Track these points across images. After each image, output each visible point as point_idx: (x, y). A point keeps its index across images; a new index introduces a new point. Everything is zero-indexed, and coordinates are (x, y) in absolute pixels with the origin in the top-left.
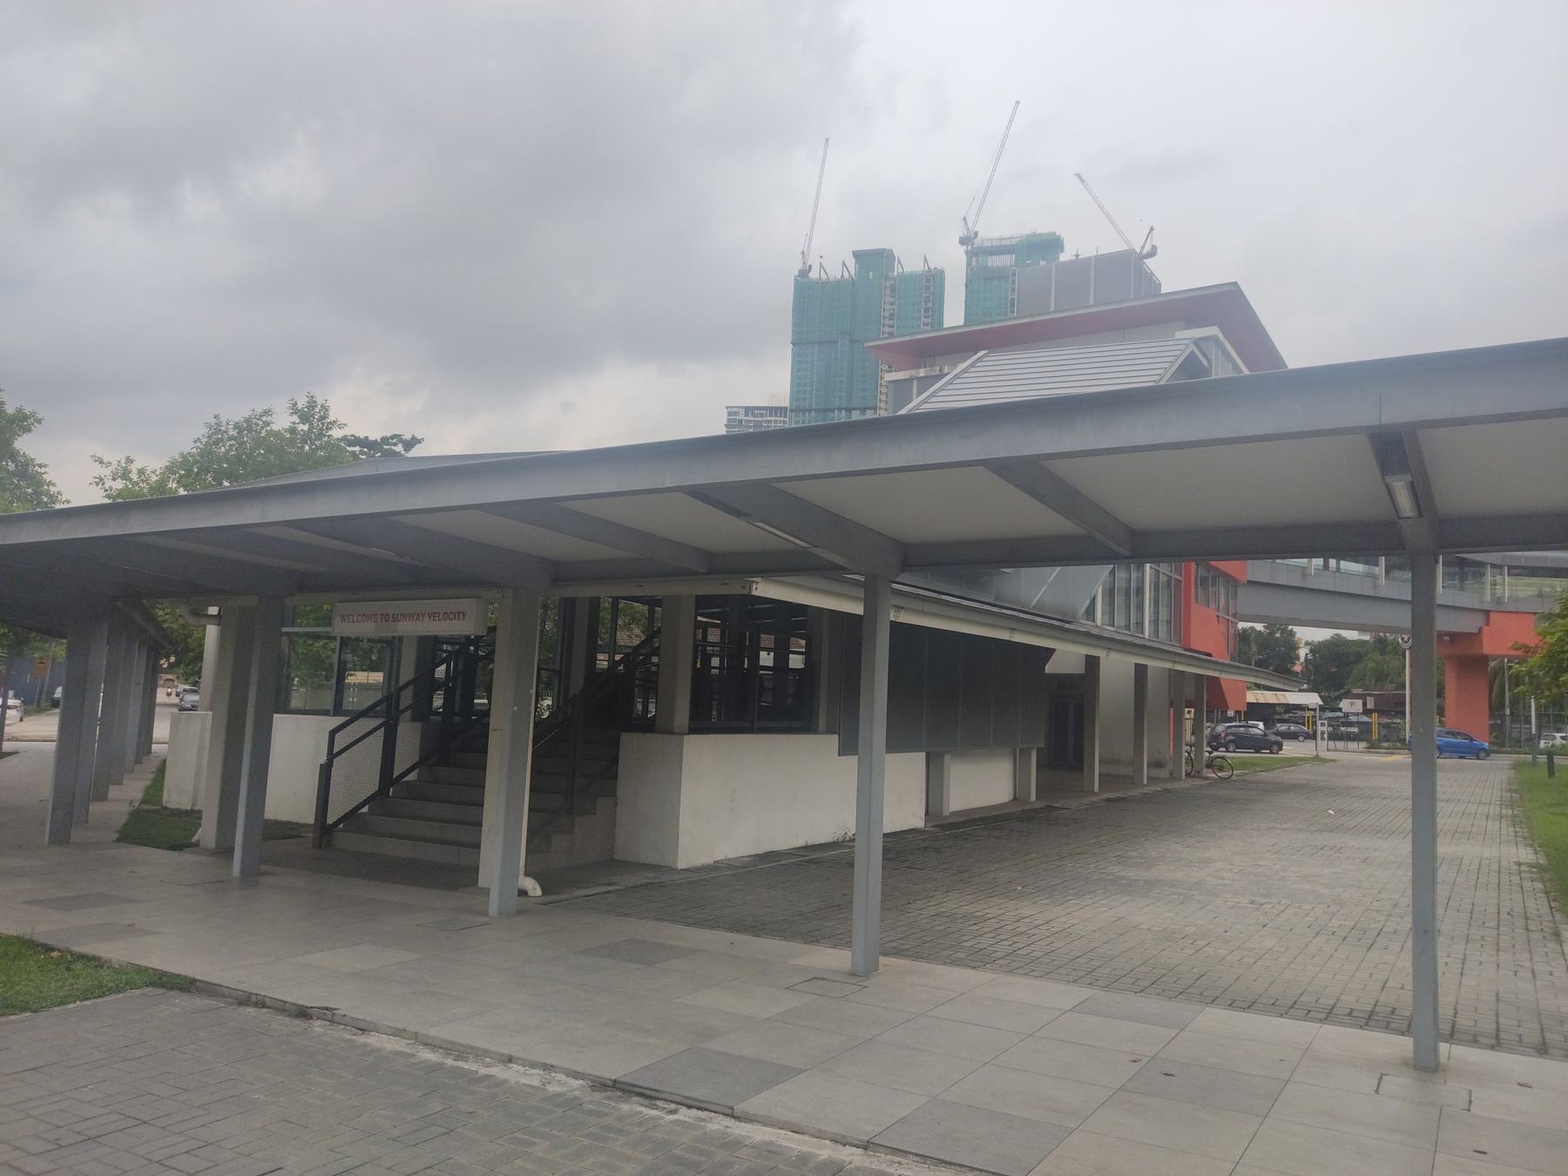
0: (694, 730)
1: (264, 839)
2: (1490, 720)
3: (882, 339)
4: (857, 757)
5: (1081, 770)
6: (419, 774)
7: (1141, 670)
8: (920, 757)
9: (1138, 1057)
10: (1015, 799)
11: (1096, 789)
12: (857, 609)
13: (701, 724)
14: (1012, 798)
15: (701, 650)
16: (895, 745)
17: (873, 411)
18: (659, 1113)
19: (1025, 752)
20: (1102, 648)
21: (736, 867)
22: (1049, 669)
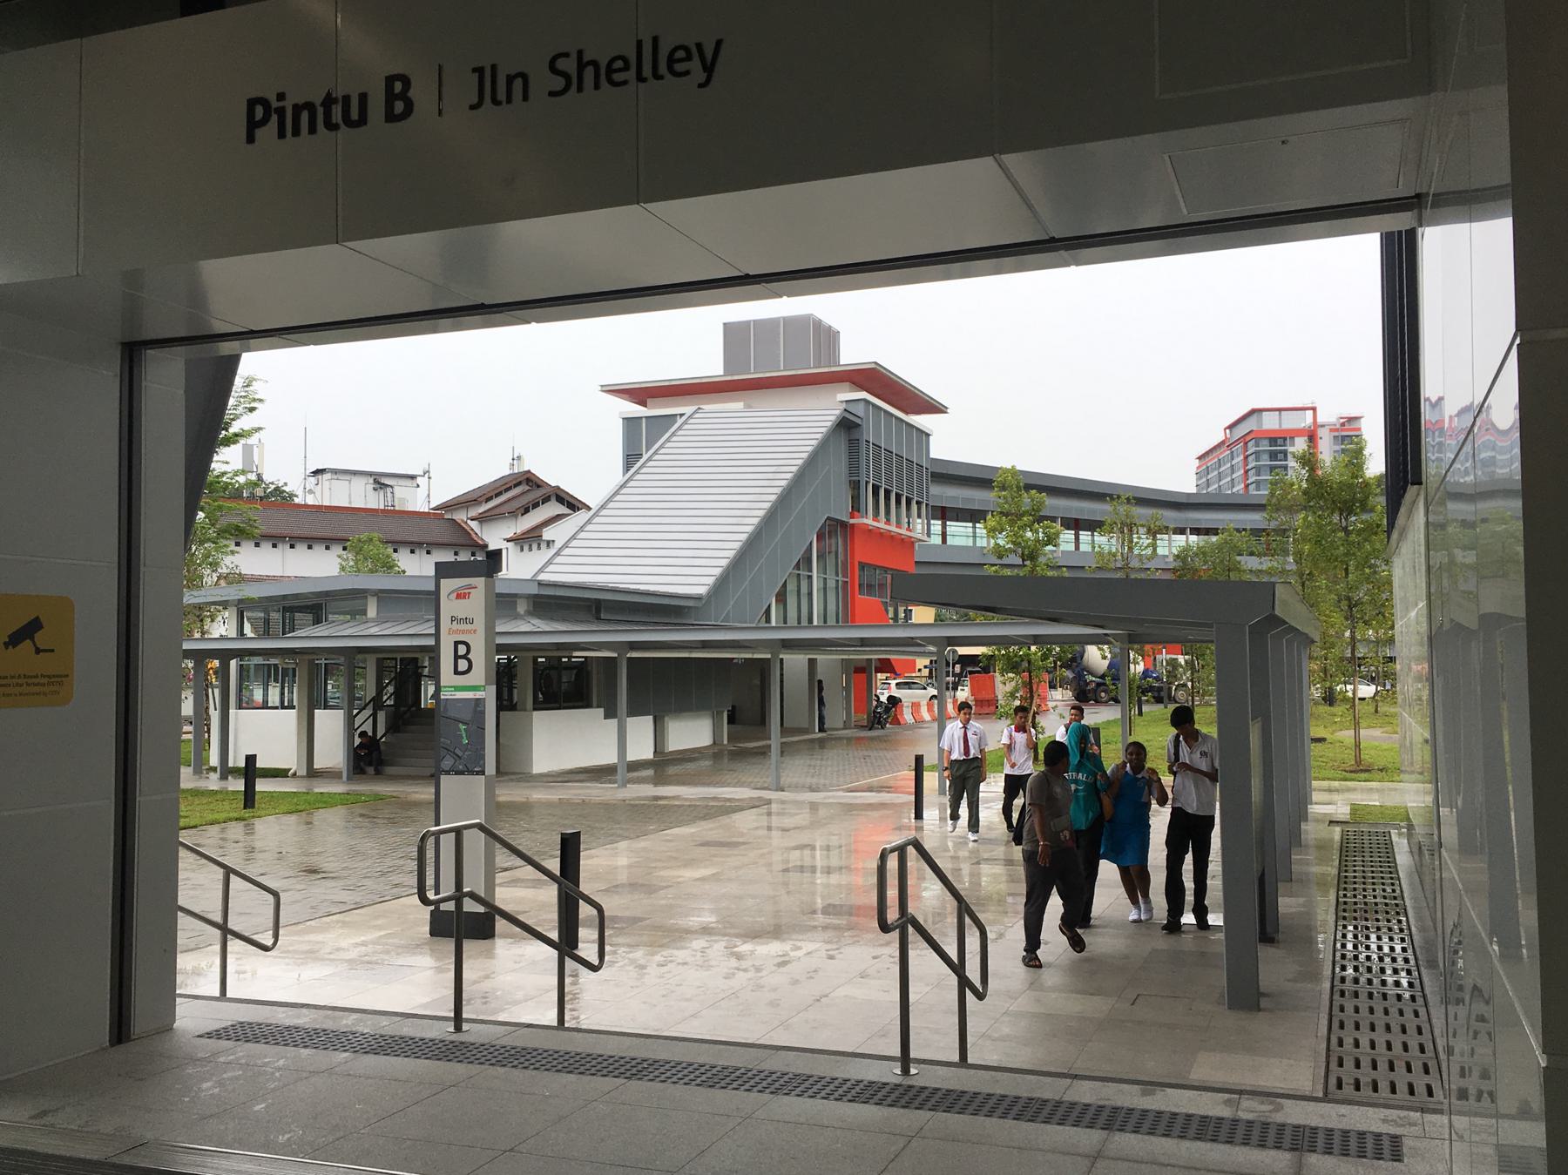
1: (1390, 1032)
2: (1334, 444)
4: (616, 720)
5: (765, 724)
7: (812, 662)
9: (782, 969)
12: (769, 656)
14: (712, 743)
16: (634, 711)
17: (310, 617)
19: (720, 713)
21: (553, 776)
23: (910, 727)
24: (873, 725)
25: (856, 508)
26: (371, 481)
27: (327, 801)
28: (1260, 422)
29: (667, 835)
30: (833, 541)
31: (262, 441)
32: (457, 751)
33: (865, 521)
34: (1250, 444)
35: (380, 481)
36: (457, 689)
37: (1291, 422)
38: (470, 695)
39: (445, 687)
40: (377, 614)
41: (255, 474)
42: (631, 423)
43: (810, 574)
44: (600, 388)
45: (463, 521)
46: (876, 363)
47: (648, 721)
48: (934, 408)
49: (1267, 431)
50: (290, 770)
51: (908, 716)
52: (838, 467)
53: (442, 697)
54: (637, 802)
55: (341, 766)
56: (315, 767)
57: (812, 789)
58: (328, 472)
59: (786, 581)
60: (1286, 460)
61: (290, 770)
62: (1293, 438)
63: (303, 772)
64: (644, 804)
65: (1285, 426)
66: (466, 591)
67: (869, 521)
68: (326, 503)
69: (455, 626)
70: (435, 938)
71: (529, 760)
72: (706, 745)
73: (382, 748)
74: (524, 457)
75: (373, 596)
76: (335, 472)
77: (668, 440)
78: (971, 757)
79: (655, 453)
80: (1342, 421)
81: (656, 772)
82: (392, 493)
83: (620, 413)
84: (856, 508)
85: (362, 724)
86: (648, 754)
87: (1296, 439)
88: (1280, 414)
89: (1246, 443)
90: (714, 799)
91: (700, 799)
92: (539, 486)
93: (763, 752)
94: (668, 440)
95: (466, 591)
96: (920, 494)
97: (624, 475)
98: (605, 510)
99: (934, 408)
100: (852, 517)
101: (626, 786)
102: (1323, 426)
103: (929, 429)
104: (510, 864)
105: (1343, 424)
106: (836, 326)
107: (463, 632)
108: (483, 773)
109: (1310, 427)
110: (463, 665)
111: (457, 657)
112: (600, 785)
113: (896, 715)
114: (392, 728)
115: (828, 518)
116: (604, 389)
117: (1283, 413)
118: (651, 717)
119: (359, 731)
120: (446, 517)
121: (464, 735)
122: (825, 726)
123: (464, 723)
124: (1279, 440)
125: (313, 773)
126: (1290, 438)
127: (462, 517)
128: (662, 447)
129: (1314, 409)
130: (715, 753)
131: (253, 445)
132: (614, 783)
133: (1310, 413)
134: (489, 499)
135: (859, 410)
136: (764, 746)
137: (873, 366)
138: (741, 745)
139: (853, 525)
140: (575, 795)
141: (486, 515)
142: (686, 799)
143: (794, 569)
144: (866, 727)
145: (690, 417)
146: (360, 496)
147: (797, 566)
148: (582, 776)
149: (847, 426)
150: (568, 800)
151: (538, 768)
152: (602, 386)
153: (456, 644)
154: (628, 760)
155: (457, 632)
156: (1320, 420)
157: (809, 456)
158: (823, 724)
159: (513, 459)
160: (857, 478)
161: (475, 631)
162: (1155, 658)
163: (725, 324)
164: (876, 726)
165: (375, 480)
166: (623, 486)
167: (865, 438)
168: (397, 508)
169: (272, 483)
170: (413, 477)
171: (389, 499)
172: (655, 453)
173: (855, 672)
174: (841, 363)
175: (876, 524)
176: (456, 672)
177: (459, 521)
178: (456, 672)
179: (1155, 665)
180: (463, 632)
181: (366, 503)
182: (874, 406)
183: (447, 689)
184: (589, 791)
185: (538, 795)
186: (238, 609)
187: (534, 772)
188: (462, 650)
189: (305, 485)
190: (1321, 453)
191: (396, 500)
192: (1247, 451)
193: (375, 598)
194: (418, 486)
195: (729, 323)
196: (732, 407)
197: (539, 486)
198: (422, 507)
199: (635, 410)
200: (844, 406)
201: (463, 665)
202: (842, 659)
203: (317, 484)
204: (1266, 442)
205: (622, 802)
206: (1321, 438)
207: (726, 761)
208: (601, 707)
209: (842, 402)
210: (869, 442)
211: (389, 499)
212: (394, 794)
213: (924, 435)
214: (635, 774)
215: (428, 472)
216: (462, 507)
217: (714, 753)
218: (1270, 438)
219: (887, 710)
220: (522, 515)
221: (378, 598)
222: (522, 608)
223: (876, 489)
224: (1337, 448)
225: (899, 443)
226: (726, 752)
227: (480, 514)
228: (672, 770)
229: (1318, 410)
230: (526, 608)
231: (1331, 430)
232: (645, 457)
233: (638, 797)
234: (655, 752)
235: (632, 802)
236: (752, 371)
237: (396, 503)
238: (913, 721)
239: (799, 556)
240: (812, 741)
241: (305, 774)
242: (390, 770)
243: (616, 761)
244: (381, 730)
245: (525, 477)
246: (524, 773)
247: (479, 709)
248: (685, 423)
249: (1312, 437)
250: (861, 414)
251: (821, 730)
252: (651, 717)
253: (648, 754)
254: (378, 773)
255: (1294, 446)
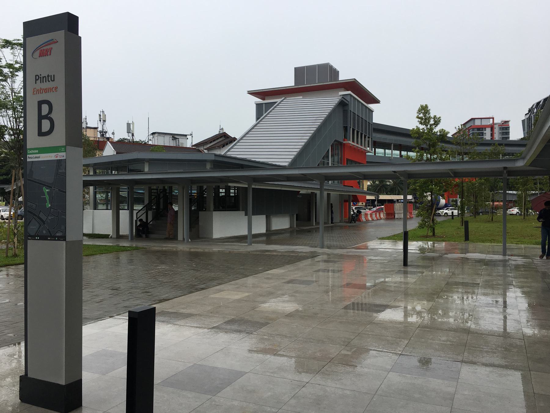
0: (214, 211)
2: (500, 130)
3: (500, 161)
6: (152, 222)
8: (264, 216)
10: (291, 227)
11: (314, 225)
13: (217, 209)
14: (290, 227)
15: (318, 182)
16: (257, 212)
18: (229, 297)
19: (293, 215)
20: (306, 189)
22: (145, 221)
23: (365, 223)
24: (351, 222)
25: (346, 137)
26: (171, 137)
27: (124, 249)
28: (474, 123)
29: (268, 274)
30: (337, 151)
31: (133, 122)
32: (42, 216)
33: (349, 142)
34: (471, 130)
35: (174, 137)
36: (42, 150)
37: (485, 123)
38: (51, 157)
39: (31, 149)
40: (149, 170)
41: (131, 133)
42: (259, 106)
43: (328, 162)
44: (247, 92)
45: (202, 150)
46: (355, 79)
47: (264, 217)
48: (376, 101)
49: (477, 126)
50: (110, 235)
51: (363, 219)
52: (338, 121)
53: (28, 160)
54: (255, 253)
55: (128, 234)
56: (120, 234)
57: (341, 248)
58: (157, 133)
59: (319, 163)
60: (483, 136)
61: (110, 235)
62: (486, 128)
63: (115, 236)
64: (258, 254)
65: (483, 124)
66: (48, 47)
67: (351, 142)
68: (156, 144)
69: (39, 85)
70: (23, 404)
71: (212, 233)
72: (287, 228)
73: (149, 226)
74: (224, 129)
75: (147, 162)
76: (159, 133)
77: (273, 109)
78: (507, 234)
79: (268, 114)
80: (503, 122)
81: (267, 238)
82: (179, 141)
83: (255, 102)
84: (346, 137)
85: (141, 216)
86: (263, 231)
87: (487, 129)
88: (481, 120)
89: (469, 130)
90: (293, 252)
91: (286, 252)
92: (228, 138)
93: (317, 230)
94: (273, 109)
95: (48, 47)
96: (369, 134)
97: (256, 121)
98: (248, 135)
99: (376, 101)
100: (344, 140)
101: (251, 245)
102: (496, 124)
103: (373, 109)
104: (167, 295)
105: (503, 123)
106: (338, 69)
107: (46, 91)
108: (63, 238)
109: (491, 124)
110: (46, 125)
111: (41, 118)
112: (240, 244)
113: (359, 218)
114: (155, 218)
115: (335, 141)
116: (249, 92)
117: (482, 119)
118: (265, 216)
119: (139, 219)
120: (196, 149)
121: (47, 199)
122: (333, 222)
123: (48, 187)
124: (481, 129)
125: (119, 237)
126: (485, 128)
127: (201, 149)
128: (270, 112)
129: (493, 118)
130: (291, 231)
131: (130, 123)
132: (246, 243)
133: (491, 120)
134: (211, 142)
135: (348, 98)
136: (310, 229)
137: (354, 80)
138: (301, 228)
139: (344, 144)
140: (227, 249)
141: (210, 148)
142: (279, 252)
143: (322, 159)
144: (348, 222)
145: (280, 103)
146: (168, 142)
147: (323, 158)
148: (233, 240)
149: (343, 104)
150: (222, 251)
151: (216, 235)
152: (248, 91)
153: (40, 103)
154: (252, 233)
155: (40, 91)
156: (495, 122)
157: (329, 114)
158: (333, 221)
159: (220, 130)
160: (346, 125)
161: (56, 88)
162: (449, 200)
163: (295, 68)
164: (352, 222)
165: (172, 136)
166: (255, 126)
167: (350, 109)
168: (180, 146)
169: (143, 141)
170: (186, 135)
171: (177, 143)
172: (268, 114)
173: (344, 202)
174: (339, 80)
175: (353, 144)
176: (41, 134)
177: (201, 150)
178: (41, 134)
179: (449, 202)
180: (46, 91)
181: (169, 144)
182: (354, 97)
183: (33, 151)
184: (234, 247)
185: (216, 249)
186: (93, 168)
187: (214, 238)
188: (45, 109)
189: (148, 138)
190: (495, 133)
191: (180, 143)
192: (469, 133)
193: (148, 163)
194: (187, 139)
195: (297, 68)
196: (298, 100)
197: (228, 138)
198: (189, 145)
199: (259, 100)
200: (342, 96)
201: (46, 125)
202: (340, 194)
203: (153, 138)
204: (476, 130)
205: (248, 253)
206: (495, 128)
207: (295, 234)
208: (244, 211)
209: (341, 95)
210: (351, 111)
211: (177, 143)
212: (144, 247)
213: (371, 111)
214: (257, 239)
215: (192, 135)
216: (202, 145)
217: (291, 231)
218: (478, 128)
219: (357, 216)
220: (222, 147)
221: (149, 163)
222: (208, 166)
223: (353, 130)
224: (501, 131)
225: (362, 113)
226: (295, 231)
227: (208, 147)
228: (274, 238)
229: (495, 119)
230: (210, 167)
231: (499, 125)
232: (264, 115)
233: (257, 250)
234: (267, 230)
235: (253, 253)
236: (305, 84)
237: (180, 145)
238: (365, 220)
239: (324, 154)
240: (329, 227)
241: (116, 237)
242: (152, 236)
243: (247, 234)
244: (150, 218)
245: (224, 134)
246: (209, 238)
247: (60, 171)
248: (278, 105)
249: (492, 127)
250: (349, 100)
251: (332, 223)
252: (265, 216)
253: (263, 231)
254: (147, 237)
255: (486, 131)
